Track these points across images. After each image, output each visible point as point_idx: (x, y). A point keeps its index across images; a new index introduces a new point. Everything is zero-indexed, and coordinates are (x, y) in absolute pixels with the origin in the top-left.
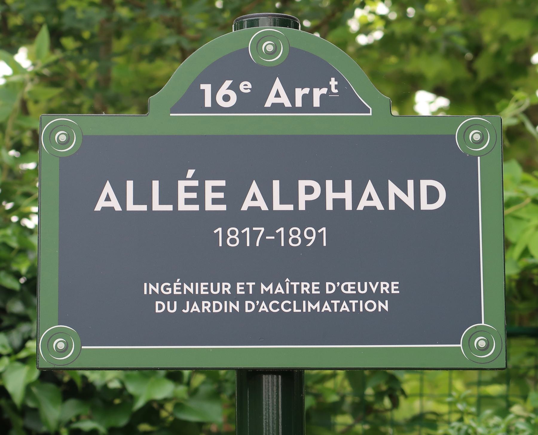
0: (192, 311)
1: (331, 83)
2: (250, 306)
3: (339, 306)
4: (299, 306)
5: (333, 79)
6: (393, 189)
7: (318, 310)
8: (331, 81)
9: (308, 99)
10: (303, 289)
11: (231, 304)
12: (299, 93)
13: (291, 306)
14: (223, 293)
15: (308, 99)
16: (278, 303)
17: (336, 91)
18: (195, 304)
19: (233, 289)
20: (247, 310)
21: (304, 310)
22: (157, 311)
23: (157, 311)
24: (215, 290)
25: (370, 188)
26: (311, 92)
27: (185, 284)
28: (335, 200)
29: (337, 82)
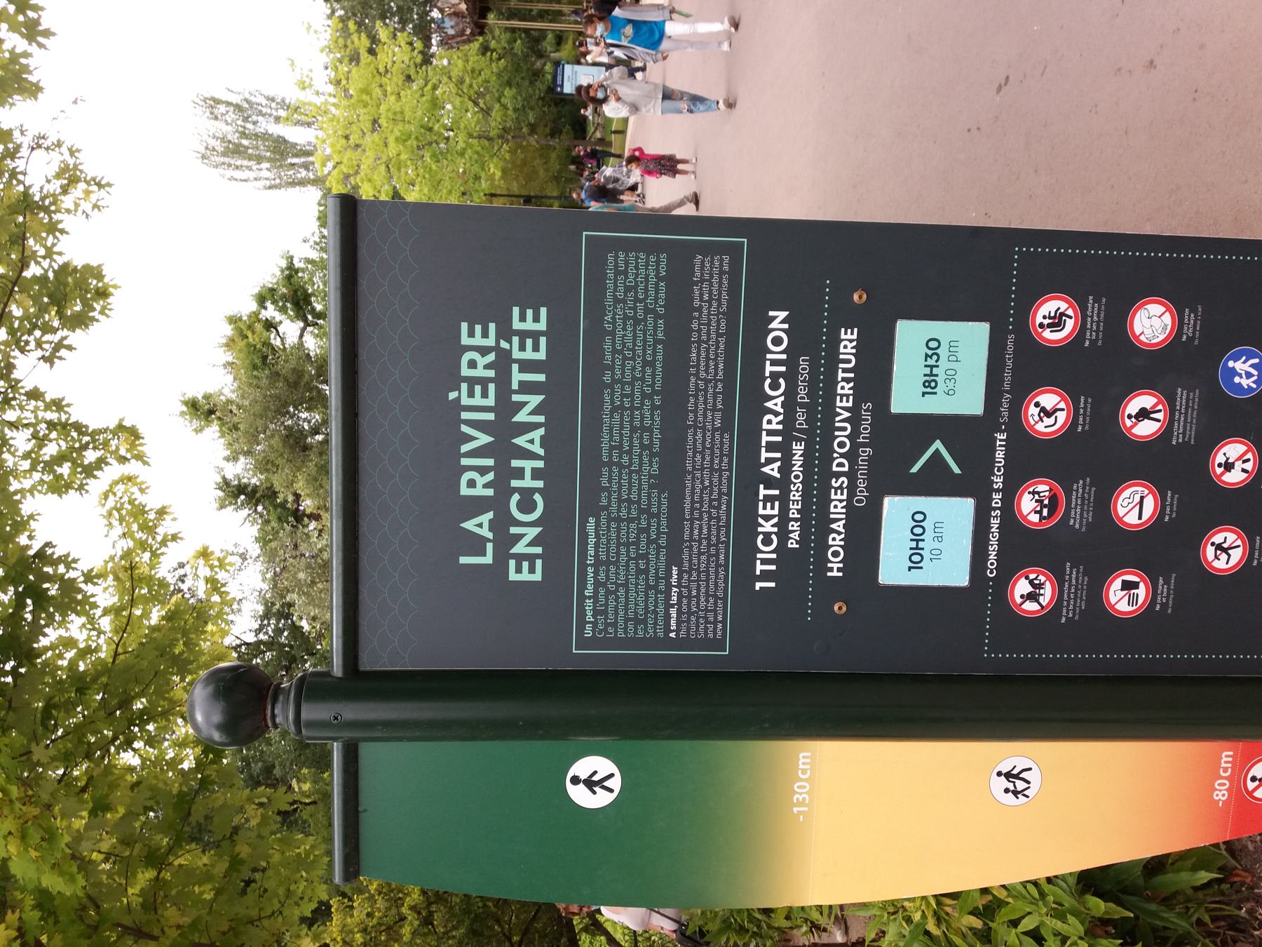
10: (774, 426)
13: (999, 467)
14: (854, 351)
24: (1001, 462)
27: (514, 551)
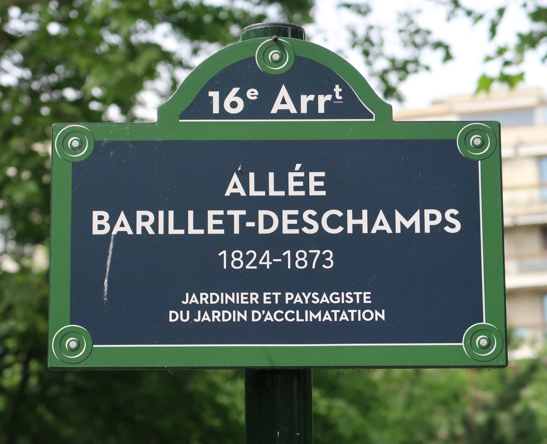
0: (202, 321)
1: (335, 90)
2: (256, 316)
3: (339, 315)
4: (302, 316)
5: (337, 86)
6: (399, 218)
7: (320, 320)
8: (335, 88)
9: (313, 105)
11: (239, 314)
12: (305, 100)
13: (294, 316)
15: (313, 105)
16: (282, 312)
17: (340, 98)
18: (206, 314)
19: (261, 299)
20: (253, 320)
21: (307, 320)
22: (171, 320)
23: (171, 320)
25: (381, 216)
26: (316, 99)
28: (354, 226)
29: (341, 89)
